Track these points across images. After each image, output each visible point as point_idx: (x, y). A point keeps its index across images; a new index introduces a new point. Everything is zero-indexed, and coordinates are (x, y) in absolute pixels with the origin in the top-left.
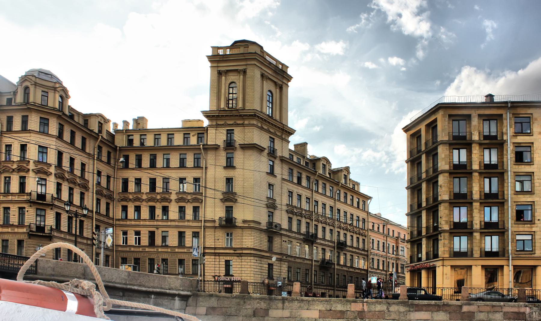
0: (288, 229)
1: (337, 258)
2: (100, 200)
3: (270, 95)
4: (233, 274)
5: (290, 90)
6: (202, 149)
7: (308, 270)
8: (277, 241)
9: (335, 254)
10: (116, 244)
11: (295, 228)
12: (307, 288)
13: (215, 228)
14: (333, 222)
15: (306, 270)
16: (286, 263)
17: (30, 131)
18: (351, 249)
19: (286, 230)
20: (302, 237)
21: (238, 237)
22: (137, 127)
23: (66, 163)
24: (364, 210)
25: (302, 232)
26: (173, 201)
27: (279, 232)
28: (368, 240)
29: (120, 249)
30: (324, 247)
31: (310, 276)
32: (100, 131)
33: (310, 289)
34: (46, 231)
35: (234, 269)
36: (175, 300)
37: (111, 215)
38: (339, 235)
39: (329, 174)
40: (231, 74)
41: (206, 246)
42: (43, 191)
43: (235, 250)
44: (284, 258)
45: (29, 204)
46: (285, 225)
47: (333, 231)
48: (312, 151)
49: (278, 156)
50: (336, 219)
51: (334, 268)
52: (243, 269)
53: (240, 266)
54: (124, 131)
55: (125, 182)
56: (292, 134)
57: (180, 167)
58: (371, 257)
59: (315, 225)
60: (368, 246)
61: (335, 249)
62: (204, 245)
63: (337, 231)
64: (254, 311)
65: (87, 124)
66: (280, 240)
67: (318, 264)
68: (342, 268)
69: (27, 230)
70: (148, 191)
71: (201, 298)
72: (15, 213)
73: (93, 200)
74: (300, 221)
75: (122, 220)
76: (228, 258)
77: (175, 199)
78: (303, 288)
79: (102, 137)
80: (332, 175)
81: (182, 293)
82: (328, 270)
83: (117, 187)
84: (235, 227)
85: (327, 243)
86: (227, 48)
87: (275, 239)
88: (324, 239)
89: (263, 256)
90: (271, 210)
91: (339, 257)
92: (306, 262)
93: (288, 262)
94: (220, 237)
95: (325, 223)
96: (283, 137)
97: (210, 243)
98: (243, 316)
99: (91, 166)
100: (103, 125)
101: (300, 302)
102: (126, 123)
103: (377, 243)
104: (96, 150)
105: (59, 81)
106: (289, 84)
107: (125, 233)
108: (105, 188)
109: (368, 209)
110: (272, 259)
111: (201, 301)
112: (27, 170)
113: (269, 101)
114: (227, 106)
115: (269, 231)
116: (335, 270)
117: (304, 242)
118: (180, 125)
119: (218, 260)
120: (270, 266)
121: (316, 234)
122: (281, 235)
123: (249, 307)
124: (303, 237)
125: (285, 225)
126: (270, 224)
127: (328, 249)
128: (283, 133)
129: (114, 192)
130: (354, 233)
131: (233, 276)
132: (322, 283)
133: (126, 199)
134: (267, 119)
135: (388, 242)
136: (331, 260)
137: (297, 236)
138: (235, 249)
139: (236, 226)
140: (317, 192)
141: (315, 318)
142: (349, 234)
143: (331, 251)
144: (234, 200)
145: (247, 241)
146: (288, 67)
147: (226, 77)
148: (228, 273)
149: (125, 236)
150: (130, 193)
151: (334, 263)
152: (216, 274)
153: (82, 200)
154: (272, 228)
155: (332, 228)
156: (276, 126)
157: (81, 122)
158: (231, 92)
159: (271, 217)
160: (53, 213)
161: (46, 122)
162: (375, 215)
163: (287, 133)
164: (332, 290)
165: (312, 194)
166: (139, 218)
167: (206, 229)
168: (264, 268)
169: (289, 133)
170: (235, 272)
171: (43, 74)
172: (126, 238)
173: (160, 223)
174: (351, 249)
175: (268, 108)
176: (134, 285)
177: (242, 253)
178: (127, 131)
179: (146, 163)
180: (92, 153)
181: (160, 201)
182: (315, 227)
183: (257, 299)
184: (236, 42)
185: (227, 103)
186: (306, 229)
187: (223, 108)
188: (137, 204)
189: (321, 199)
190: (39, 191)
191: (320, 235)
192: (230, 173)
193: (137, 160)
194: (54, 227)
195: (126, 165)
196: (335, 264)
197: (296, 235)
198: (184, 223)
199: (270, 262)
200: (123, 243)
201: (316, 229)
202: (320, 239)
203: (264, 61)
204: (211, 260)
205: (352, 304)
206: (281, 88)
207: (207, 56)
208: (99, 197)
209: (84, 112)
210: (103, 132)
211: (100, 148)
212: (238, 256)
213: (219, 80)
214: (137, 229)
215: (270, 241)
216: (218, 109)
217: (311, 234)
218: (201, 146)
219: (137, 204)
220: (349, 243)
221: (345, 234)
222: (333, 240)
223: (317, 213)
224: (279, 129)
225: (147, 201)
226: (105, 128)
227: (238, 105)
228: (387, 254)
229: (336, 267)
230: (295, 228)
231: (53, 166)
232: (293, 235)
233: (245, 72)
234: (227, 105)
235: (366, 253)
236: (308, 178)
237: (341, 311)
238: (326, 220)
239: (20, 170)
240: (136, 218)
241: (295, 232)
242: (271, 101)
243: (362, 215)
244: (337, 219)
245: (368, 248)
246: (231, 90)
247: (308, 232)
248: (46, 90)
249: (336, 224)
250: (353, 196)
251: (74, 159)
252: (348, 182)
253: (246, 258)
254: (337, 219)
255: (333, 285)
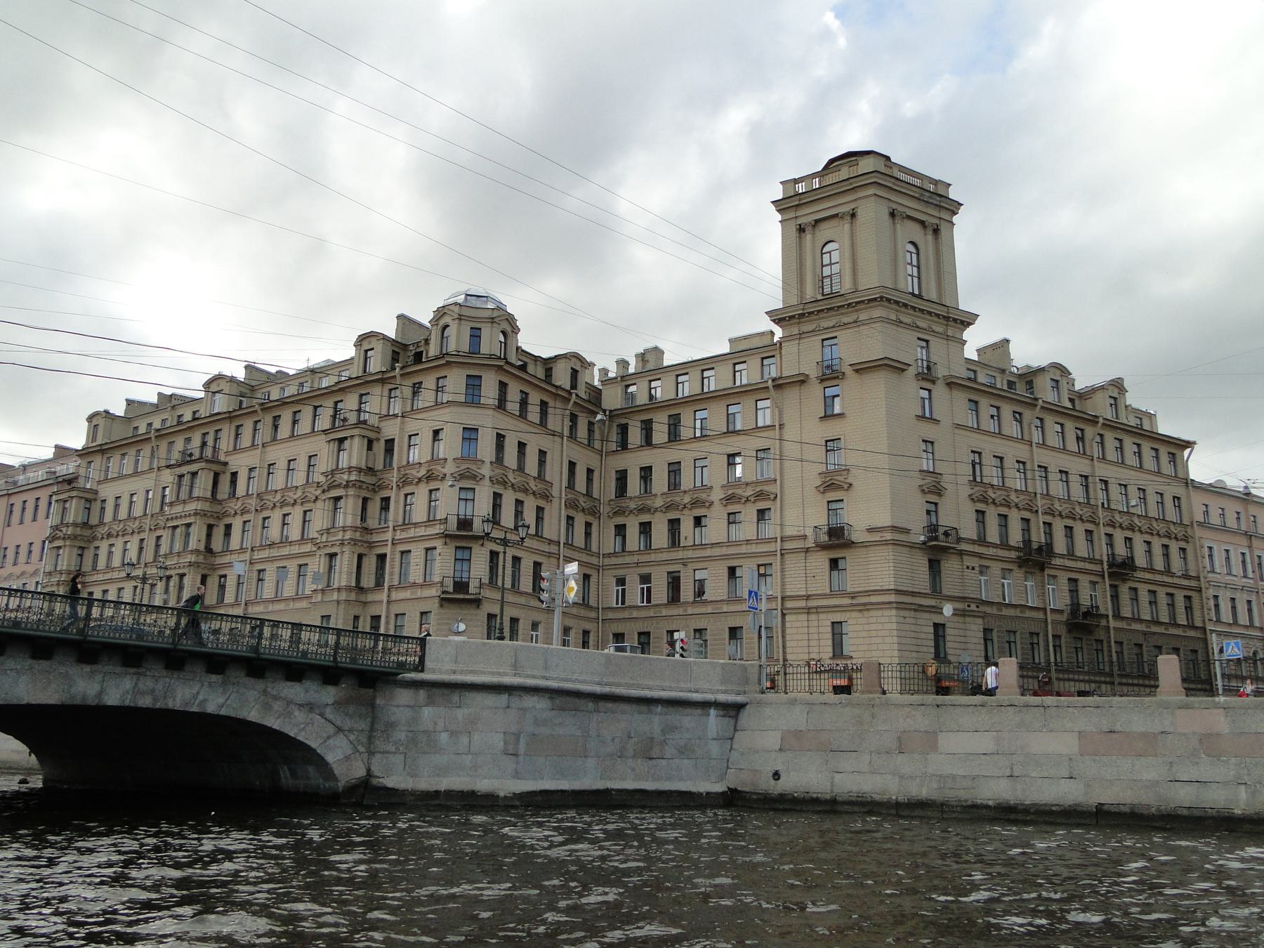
0: (999, 543)
1: (1112, 600)
2: (572, 518)
3: (914, 250)
4: (851, 654)
5: (957, 231)
6: (771, 387)
7: (1038, 634)
8: (950, 566)
9: (1106, 591)
10: (604, 606)
11: (993, 535)
12: (1039, 681)
13: (806, 552)
14: (1093, 513)
15: (1032, 634)
16: (980, 621)
17: (656, 447)
18: (1148, 576)
19: (973, 542)
20: (1013, 554)
21: (859, 567)
22: (643, 367)
23: (511, 457)
24: (1084, 454)
25: (1012, 543)
26: (715, 503)
27: (953, 548)
28: (1195, 550)
29: (611, 615)
30: (1073, 576)
31: (1042, 649)
32: (574, 386)
33: (1046, 683)
34: (472, 590)
35: (852, 641)
36: (709, 715)
37: (594, 548)
38: (1111, 544)
39: (1071, 400)
40: (823, 225)
41: (788, 594)
42: (469, 512)
43: (853, 598)
44: (973, 607)
45: (443, 540)
46: (968, 529)
47: (1032, 524)
48: (1025, 354)
49: (940, 376)
50: (1100, 505)
51: (1108, 628)
52: (873, 641)
53: (865, 634)
54: (619, 379)
55: (622, 477)
56: (969, 324)
57: (670, 441)
58: (1212, 592)
59: (1044, 523)
60: (1197, 565)
61: (1104, 578)
62: (782, 592)
63: (1106, 534)
64: (899, 738)
65: (551, 375)
66: (960, 567)
67: (1064, 618)
68: (1131, 625)
69: (437, 591)
70: (666, 490)
71: (768, 710)
72: (418, 560)
73: (560, 521)
74: (1005, 517)
75: (615, 554)
76: (837, 617)
77: (721, 499)
78: (1026, 680)
79: (577, 395)
80: (1077, 402)
81: (722, 698)
82: (1090, 632)
83: (605, 488)
84: (850, 544)
85: (1080, 565)
86: (814, 176)
87: (947, 565)
88: (1071, 554)
89: (921, 606)
90: (933, 498)
91: (1115, 597)
92: (1028, 614)
93: (983, 618)
94: (816, 571)
95: (1131, 528)
96: (950, 333)
97: (796, 587)
98: (871, 753)
99: (557, 454)
100: (579, 375)
101: (1020, 711)
102: (623, 363)
103: (1224, 555)
104: (565, 423)
105: (501, 306)
106: (955, 219)
107: (621, 581)
108: (584, 494)
109: (1187, 473)
110: (942, 613)
111: (770, 716)
112: (442, 476)
113: (911, 264)
114: (821, 291)
115: (930, 546)
116: (1109, 632)
117: (1020, 567)
118: (725, 348)
119: (805, 624)
120: (939, 628)
121: (1050, 545)
122: (961, 553)
123: (887, 728)
124: (1017, 553)
125: (968, 529)
126: (933, 529)
127: (1084, 581)
128: (947, 325)
129: (600, 501)
130: (1152, 534)
131: (851, 657)
132: (1078, 667)
133: (620, 512)
134: (909, 301)
135: (1257, 553)
136: (1097, 607)
137: (1001, 553)
138: (853, 596)
139: (853, 543)
140: (1103, 458)
141: (1067, 755)
142: (1138, 540)
143: (1094, 583)
144: (846, 486)
145: (879, 573)
146: (950, 185)
147: (814, 234)
148: (838, 651)
149: (645, 586)
150: (631, 498)
151: (1105, 613)
152: (812, 656)
153: (540, 523)
154: (936, 539)
155: (1090, 527)
156: (930, 313)
157: (541, 373)
158: (826, 261)
159: (933, 514)
160: (484, 552)
161: (477, 383)
162: (1210, 485)
163: (890, 303)
164: (1105, 683)
165: (1032, 451)
166: (648, 546)
167: (786, 556)
168: (923, 636)
169: (962, 322)
170: (855, 648)
171: (473, 298)
172: (624, 590)
173: (690, 554)
174: (1148, 576)
175: (910, 278)
176: (619, 685)
177: (872, 604)
178: (625, 379)
179: (660, 435)
180: (558, 429)
181: (690, 507)
182: (1045, 528)
183: (903, 706)
184: (832, 161)
185: (821, 285)
186: (1023, 535)
187: (813, 297)
188: (645, 518)
189: (1055, 462)
190: (462, 513)
191: (1060, 546)
192: (832, 429)
193: (644, 431)
194: (486, 580)
195: (624, 445)
196: (1107, 616)
197: (999, 550)
198: (738, 548)
199: (938, 619)
200: (617, 603)
201: (1049, 534)
202: (1062, 556)
203: (894, 184)
204: (799, 624)
205: (1179, 712)
206: (936, 231)
207: (773, 202)
208: (572, 513)
209: (546, 354)
210: (579, 387)
211: (574, 418)
212: (860, 611)
213: (800, 243)
214: (645, 570)
215: (934, 566)
216: (801, 301)
217: (1035, 546)
218: (770, 382)
219: (645, 518)
220: (1140, 561)
221: (1128, 540)
222: (1097, 557)
223: (1069, 499)
224: (939, 318)
225: (664, 510)
226: (584, 378)
227: (843, 284)
228: (1256, 582)
229: (1113, 623)
230: (993, 535)
231: (488, 465)
232: (991, 551)
233: (853, 215)
234: (821, 289)
235: (1193, 583)
236: (1018, 417)
237: (1145, 735)
238: (1074, 509)
239: (430, 477)
240: (642, 549)
241: (995, 546)
242: (915, 263)
243: (1171, 490)
244: (1103, 504)
245: (1198, 572)
246: (826, 257)
247: (1027, 542)
248: (478, 325)
249: (1101, 516)
250: (1139, 445)
251: (504, 436)
252: (1122, 413)
253: (879, 613)
254: (1103, 504)
255: (1107, 669)
